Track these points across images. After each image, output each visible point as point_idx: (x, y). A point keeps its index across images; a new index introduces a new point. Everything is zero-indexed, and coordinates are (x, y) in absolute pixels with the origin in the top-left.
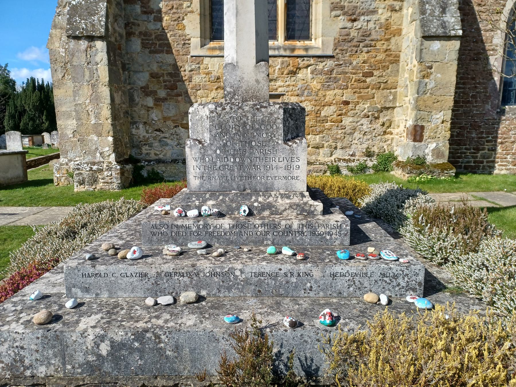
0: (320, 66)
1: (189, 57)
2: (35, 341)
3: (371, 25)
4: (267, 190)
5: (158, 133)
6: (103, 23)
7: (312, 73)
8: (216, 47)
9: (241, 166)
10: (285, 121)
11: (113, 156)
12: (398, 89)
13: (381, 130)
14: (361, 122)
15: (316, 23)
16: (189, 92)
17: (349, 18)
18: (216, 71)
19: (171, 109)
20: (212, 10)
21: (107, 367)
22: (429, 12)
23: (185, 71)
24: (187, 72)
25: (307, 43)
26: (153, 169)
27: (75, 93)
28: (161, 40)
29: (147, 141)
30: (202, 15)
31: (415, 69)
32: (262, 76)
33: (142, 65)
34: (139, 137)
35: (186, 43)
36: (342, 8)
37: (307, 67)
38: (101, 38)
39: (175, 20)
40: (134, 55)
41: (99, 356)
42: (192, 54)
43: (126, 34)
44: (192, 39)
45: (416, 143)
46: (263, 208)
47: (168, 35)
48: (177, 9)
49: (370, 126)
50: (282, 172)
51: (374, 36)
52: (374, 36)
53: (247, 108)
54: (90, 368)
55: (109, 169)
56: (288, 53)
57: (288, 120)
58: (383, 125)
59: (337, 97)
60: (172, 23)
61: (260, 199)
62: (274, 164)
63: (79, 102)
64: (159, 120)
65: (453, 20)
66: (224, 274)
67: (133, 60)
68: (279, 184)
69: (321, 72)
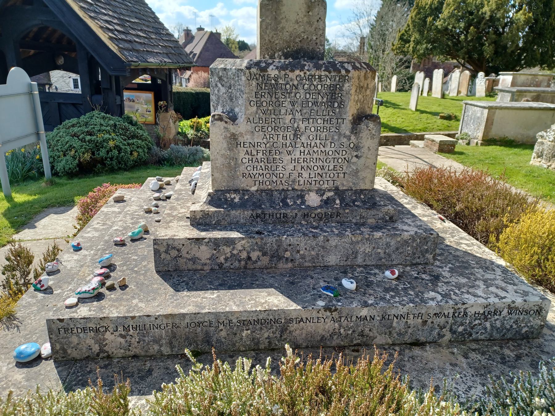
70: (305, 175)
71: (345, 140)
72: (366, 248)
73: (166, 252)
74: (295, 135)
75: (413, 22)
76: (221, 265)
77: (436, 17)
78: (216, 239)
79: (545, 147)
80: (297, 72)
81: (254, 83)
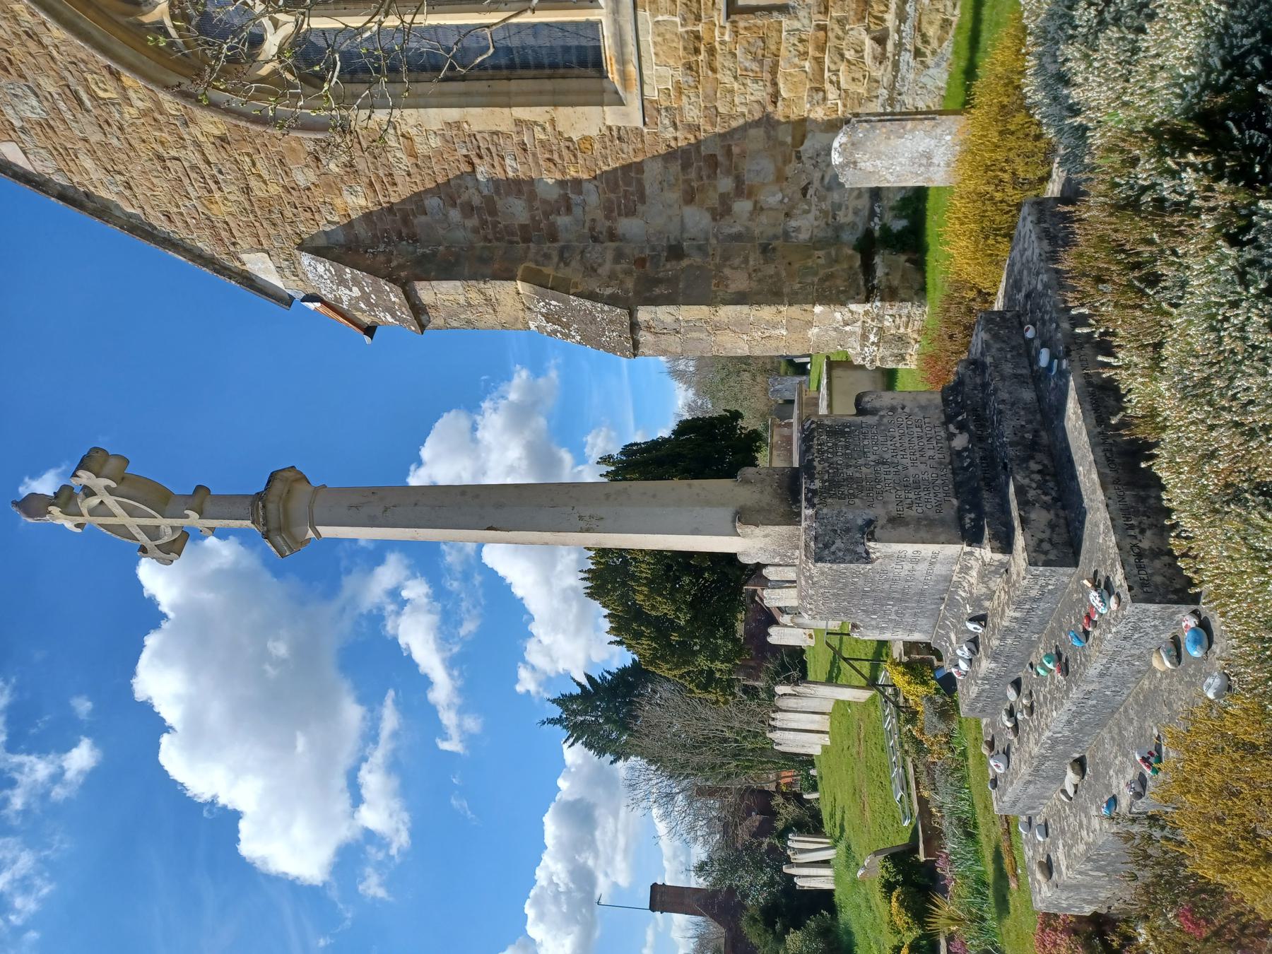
1: (646, 130)
5: (811, 192)
8: (618, 70)
16: (721, 131)
18: (671, 72)
19: (758, 168)
23: (676, 139)
26: (892, 208)
28: (616, 184)
33: (670, 218)
34: (818, 227)
35: (618, 135)
38: (632, 314)
39: (575, 156)
40: (651, 231)
42: (640, 125)
43: (612, 241)
44: (609, 123)
47: (605, 168)
48: (551, 151)
55: (880, 318)
57: (834, 553)
60: (581, 161)
64: (781, 190)
67: (660, 233)
70: (931, 453)
71: (885, 420)
72: (1008, 368)
73: (1046, 553)
74: (884, 463)
75: (677, 666)
76: (1055, 500)
77: (673, 626)
78: (1019, 504)
79: (887, 353)
80: (816, 463)
81: (829, 500)
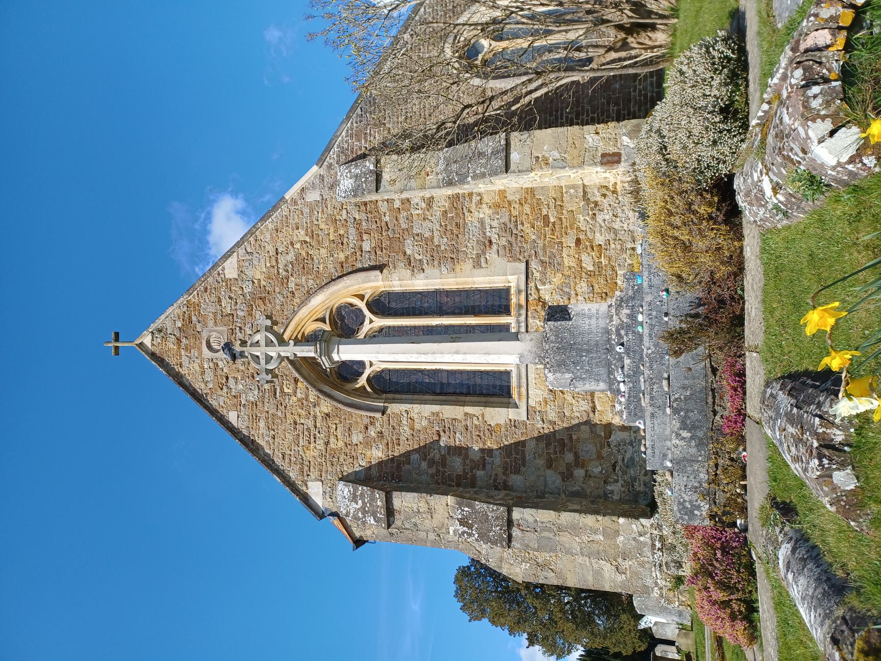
0: (537, 275)
2: (681, 476)
3: (495, 224)
4: (608, 332)
5: (618, 468)
6: (495, 508)
7: (544, 284)
9: (588, 351)
10: (556, 320)
11: (643, 520)
12: (563, 185)
13: (611, 198)
14: (601, 222)
15: (493, 283)
17: (488, 248)
19: (587, 449)
20: (481, 394)
21: (700, 434)
22: (483, 169)
24: (545, 426)
25: (513, 291)
27: (569, 552)
29: (628, 484)
30: (486, 405)
31: (539, 173)
32: (528, 337)
33: (538, 476)
34: (624, 492)
35: (514, 424)
36: (478, 256)
37: (538, 290)
38: (510, 512)
41: (691, 438)
42: (525, 419)
45: (623, 159)
46: (619, 335)
47: (506, 443)
49: (606, 211)
50: (593, 321)
51: (505, 219)
52: (505, 219)
53: (547, 347)
54: (700, 444)
55: (659, 527)
56: (523, 312)
58: (604, 195)
59: (571, 253)
61: (614, 337)
62: (587, 327)
63: (578, 549)
64: (601, 465)
65: (489, 144)
66: (651, 361)
68: (602, 323)
69: (544, 273)
